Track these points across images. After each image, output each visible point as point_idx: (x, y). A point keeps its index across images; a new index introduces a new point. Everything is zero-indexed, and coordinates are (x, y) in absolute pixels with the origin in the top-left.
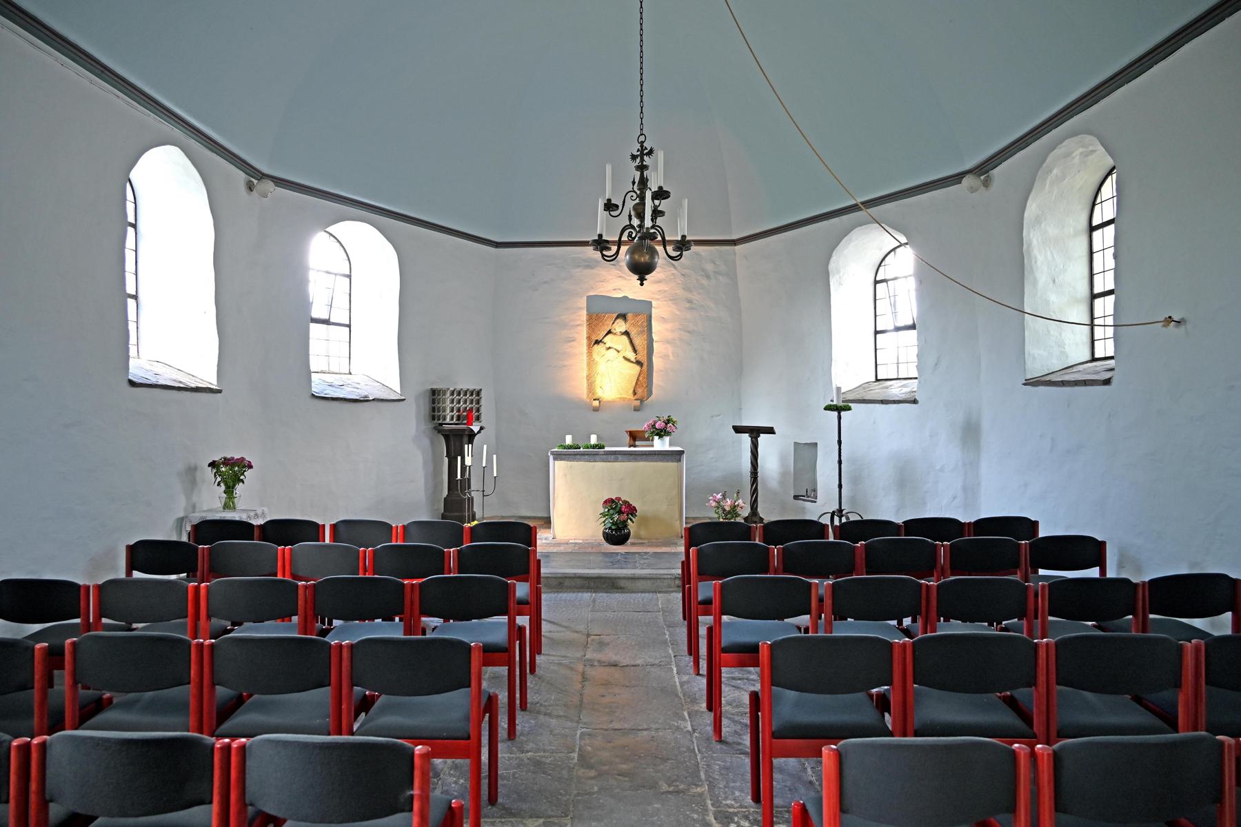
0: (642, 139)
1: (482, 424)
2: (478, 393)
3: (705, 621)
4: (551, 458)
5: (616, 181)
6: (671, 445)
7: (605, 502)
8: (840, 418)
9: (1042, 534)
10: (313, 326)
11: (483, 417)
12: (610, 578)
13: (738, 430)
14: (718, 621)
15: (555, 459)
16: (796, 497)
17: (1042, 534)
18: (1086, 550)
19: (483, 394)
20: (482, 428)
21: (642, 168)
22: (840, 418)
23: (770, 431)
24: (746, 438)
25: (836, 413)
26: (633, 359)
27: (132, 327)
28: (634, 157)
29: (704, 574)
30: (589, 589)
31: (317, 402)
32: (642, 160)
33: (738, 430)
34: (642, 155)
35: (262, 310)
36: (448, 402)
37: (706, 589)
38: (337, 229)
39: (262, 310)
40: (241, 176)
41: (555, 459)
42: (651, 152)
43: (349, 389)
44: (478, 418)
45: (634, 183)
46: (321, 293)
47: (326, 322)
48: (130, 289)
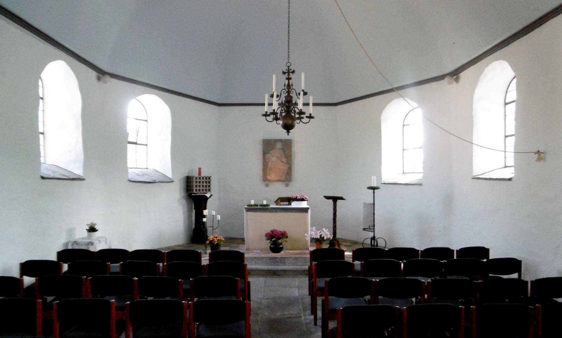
0: (289, 64)
1: (212, 193)
2: (209, 178)
3: (319, 300)
4: (245, 211)
5: (276, 84)
6: (93, 297)
7: (267, 235)
8: (374, 193)
9: (492, 256)
10: (129, 145)
11: (212, 190)
12: (273, 271)
13: (327, 198)
14: (327, 298)
15: (247, 211)
16: (364, 229)
17: (492, 256)
18: (514, 265)
19: (212, 178)
20: (211, 196)
21: (289, 79)
22: (374, 193)
23: (341, 198)
24: (331, 201)
25: (372, 191)
26: (285, 161)
27: (42, 148)
28: (284, 73)
29: (320, 275)
30: (263, 275)
31: (131, 183)
32: (289, 75)
33: (327, 198)
34: (289, 72)
35: (104, 139)
36: (194, 182)
37: (321, 283)
38: (139, 98)
39: (104, 139)
40: (93, 74)
41: (247, 211)
42: (293, 72)
43: (147, 177)
44: (209, 190)
45: (285, 85)
46: (133, 129)
47: (136, 143)
48: (41, 130)
